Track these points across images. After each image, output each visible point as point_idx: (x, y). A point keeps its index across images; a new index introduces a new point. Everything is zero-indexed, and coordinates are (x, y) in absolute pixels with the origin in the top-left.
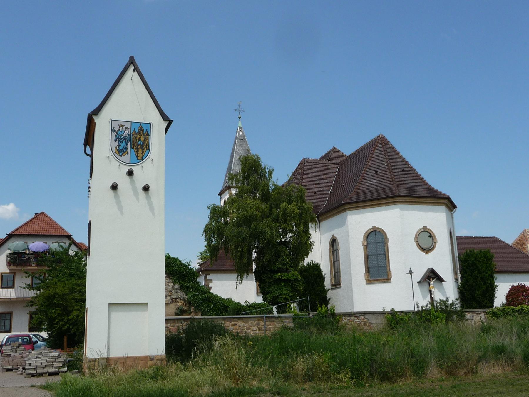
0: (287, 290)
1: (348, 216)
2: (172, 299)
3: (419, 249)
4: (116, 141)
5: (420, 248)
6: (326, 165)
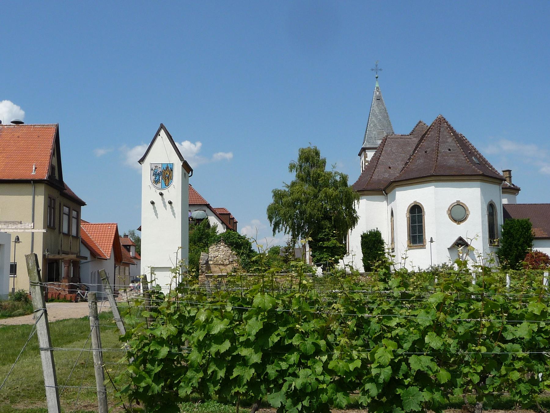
0: (328, 255)
1: (397, 192)
2: (229, 261)
3: (451, 220)
4: (153, 176)
5: (452, 219)
6: (407, 139)
